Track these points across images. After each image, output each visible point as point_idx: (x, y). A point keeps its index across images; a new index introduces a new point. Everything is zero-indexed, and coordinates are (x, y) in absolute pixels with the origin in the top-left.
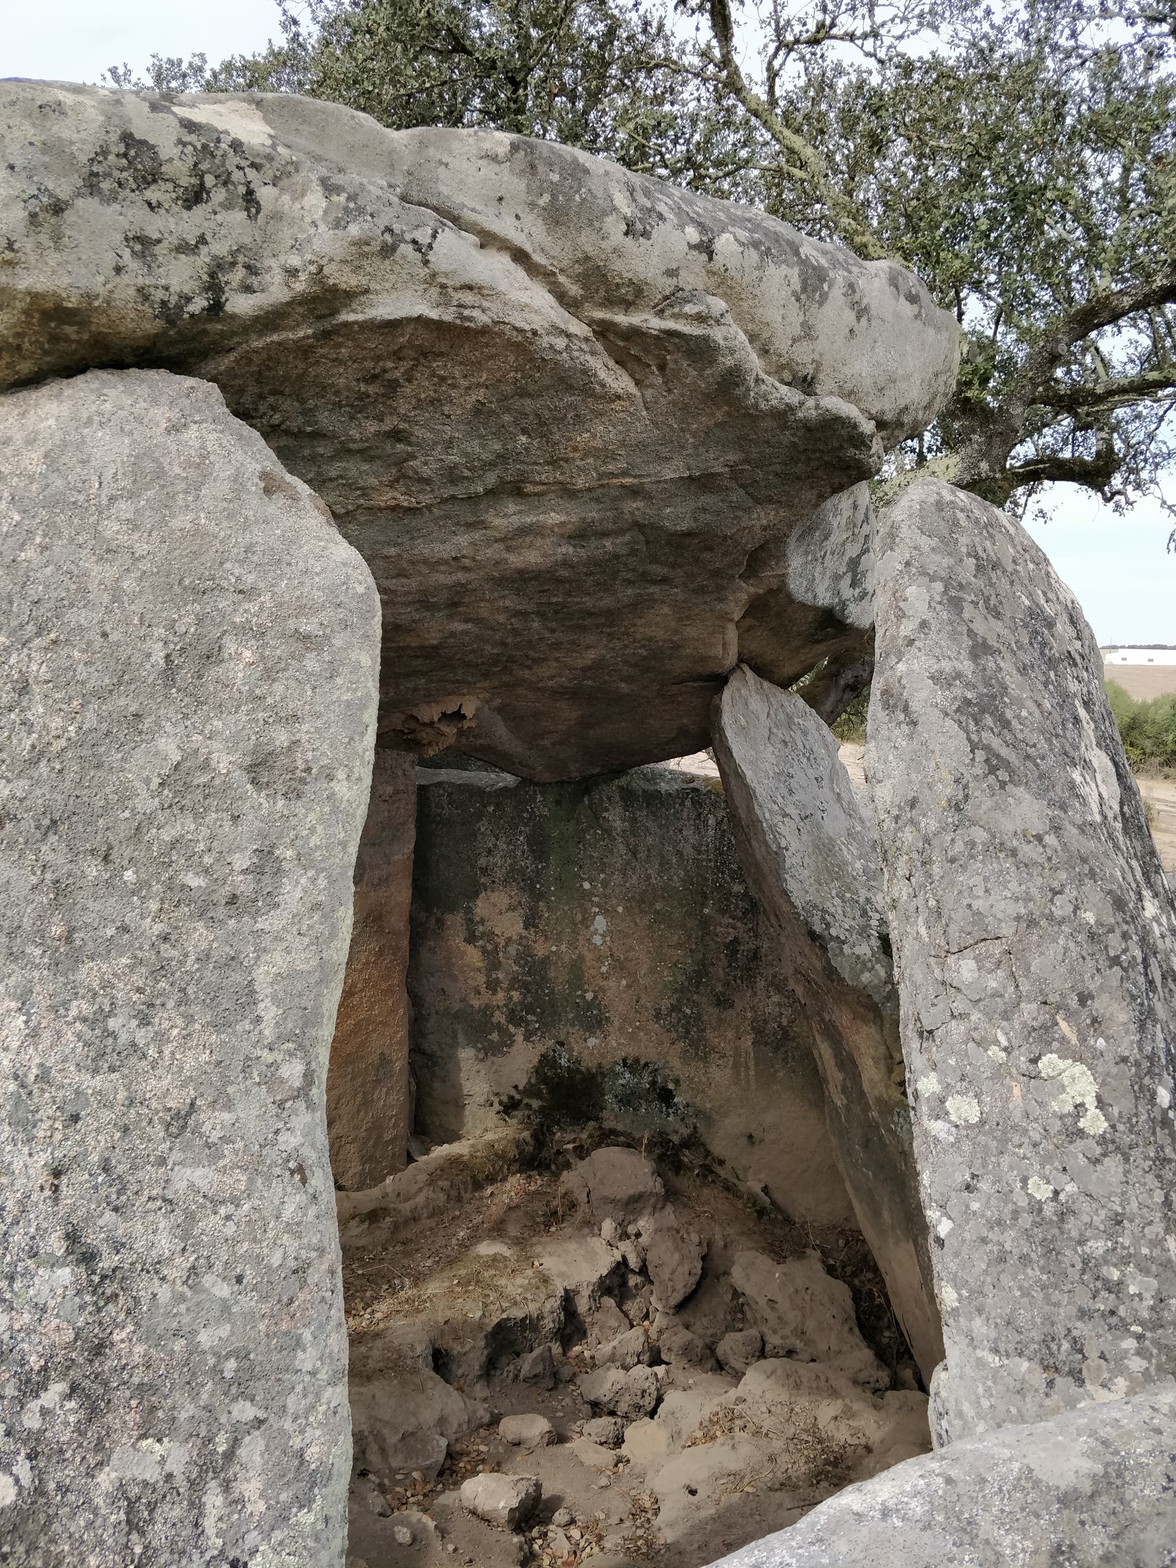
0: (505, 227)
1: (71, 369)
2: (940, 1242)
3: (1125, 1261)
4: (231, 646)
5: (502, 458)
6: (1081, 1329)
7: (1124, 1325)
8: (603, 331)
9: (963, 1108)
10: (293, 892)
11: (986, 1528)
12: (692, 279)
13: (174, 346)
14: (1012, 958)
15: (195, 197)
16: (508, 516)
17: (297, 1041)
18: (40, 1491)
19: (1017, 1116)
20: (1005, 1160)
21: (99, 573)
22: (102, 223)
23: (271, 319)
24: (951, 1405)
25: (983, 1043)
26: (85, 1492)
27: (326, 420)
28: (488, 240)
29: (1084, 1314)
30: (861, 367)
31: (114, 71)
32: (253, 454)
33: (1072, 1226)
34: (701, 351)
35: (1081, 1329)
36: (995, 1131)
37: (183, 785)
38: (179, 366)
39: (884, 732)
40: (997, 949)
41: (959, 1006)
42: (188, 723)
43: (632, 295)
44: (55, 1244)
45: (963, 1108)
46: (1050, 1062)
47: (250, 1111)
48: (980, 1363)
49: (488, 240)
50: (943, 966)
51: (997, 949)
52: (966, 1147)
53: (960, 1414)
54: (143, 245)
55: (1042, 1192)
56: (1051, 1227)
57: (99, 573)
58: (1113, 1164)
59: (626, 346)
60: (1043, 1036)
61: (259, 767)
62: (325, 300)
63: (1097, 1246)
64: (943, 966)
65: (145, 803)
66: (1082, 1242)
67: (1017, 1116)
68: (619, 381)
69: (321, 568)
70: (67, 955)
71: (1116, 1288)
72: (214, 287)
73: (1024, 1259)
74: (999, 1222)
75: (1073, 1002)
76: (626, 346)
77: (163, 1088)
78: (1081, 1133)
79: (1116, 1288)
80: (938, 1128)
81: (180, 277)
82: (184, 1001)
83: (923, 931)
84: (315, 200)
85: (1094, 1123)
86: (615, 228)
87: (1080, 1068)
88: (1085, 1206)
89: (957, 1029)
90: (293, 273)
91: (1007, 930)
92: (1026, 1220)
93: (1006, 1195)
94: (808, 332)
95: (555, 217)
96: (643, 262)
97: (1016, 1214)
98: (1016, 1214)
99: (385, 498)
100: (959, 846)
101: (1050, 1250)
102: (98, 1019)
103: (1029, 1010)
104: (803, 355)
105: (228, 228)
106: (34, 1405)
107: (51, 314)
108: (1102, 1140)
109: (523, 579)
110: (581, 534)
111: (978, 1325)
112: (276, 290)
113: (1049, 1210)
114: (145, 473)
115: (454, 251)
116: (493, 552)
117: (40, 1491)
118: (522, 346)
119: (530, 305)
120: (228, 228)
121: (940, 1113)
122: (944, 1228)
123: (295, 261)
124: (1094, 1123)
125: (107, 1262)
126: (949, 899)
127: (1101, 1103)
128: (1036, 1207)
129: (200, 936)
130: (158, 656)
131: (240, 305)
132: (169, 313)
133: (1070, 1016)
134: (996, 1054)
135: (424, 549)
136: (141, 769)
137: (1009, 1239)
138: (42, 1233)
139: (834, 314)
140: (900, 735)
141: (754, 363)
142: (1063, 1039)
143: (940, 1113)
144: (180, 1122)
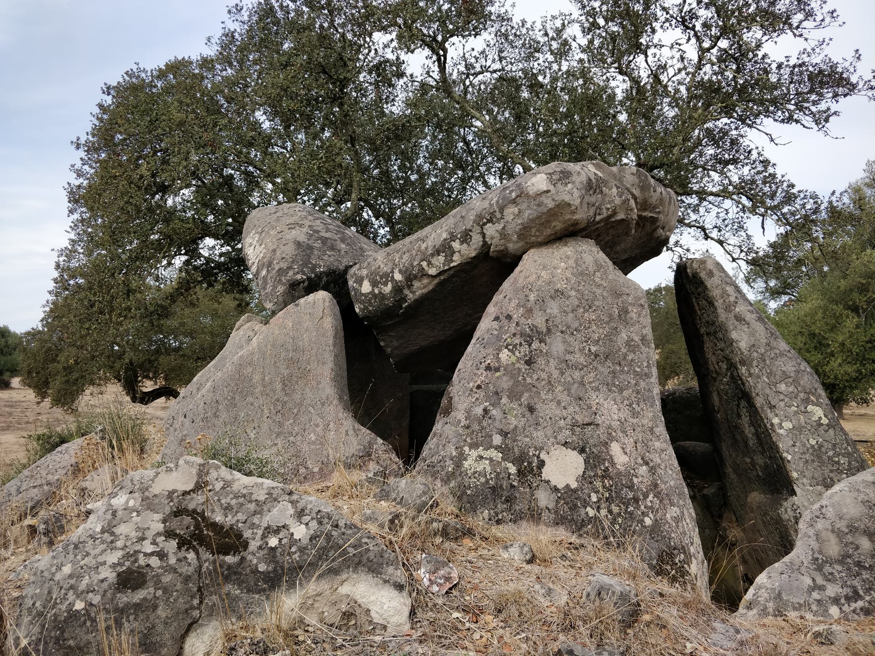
2: (788, 461)
3: (839, 455)
4: (630, 309)
6: (831, 475)
7: (842, 472)
9: (787, 425)
11: (862, 489)
14: (796, 382)
18: (656, 520)
19: (803, 424)
20: (802, 436)
21: (598, 291)
24: (800, 505)
25: (789, 407)
26: (665, 519)
29: (831, 471)
31: (127, 73)
33: (823, 449)
35: (831, 475)
36: (798, 429)
39: (739, 327)
40: (791, 380)
41: (782, 397)
44: (640, 461)
45: (787, 425)
46: (810, 408)
48: (808, 490)
50: (775, 387)
51: (791, 380)
52: (790, 435)
53: (804, 506)
55: (813, 442)
56: (818, 451)
57: (598, 291)
58: (831, 432)
60: (807, 401)
63: (831, 453)
64: (775, 387)
65: (624, 350)
66: (827, 453)
67: (803, 424)
71: (838, 463)
73: (813, 461)
74: (804, 453)
75: (813, 391)
78: (822, 424)
79: (838, 463)
80: (781, 431)
82: (644, 400)
83: (766, 380)
84: (614, 190)
85: (825, 421)
87: (818, 408)
88: (825, 444)
89: (782, 404)
90: (608, 209)
91: (792, 375)
92: (811, 451)
93: (804, 445)
97: (808, 450)
98: (808, 450)
100: (773, 355)
101: (819, 457)
102: (630, 405)
103: (802, 395)
106: (648, 500)
108: (827, 425)
111: (805, 481)
113: (816, 447)
117: (656, 520)
121: (781, 427)
122: (789, 457)
123: (609, 206)
124: (825, 421)
125: (651, 464)
126: (774, 369)
127: (825, 416)
128: (813, 447)
130: (617, 312)
133: (813, 395)
134: (794, 409)
137: (807, 456)
138: (636, 458)
140: (745, 328)
142: (813, 401)
143: (781, 427)
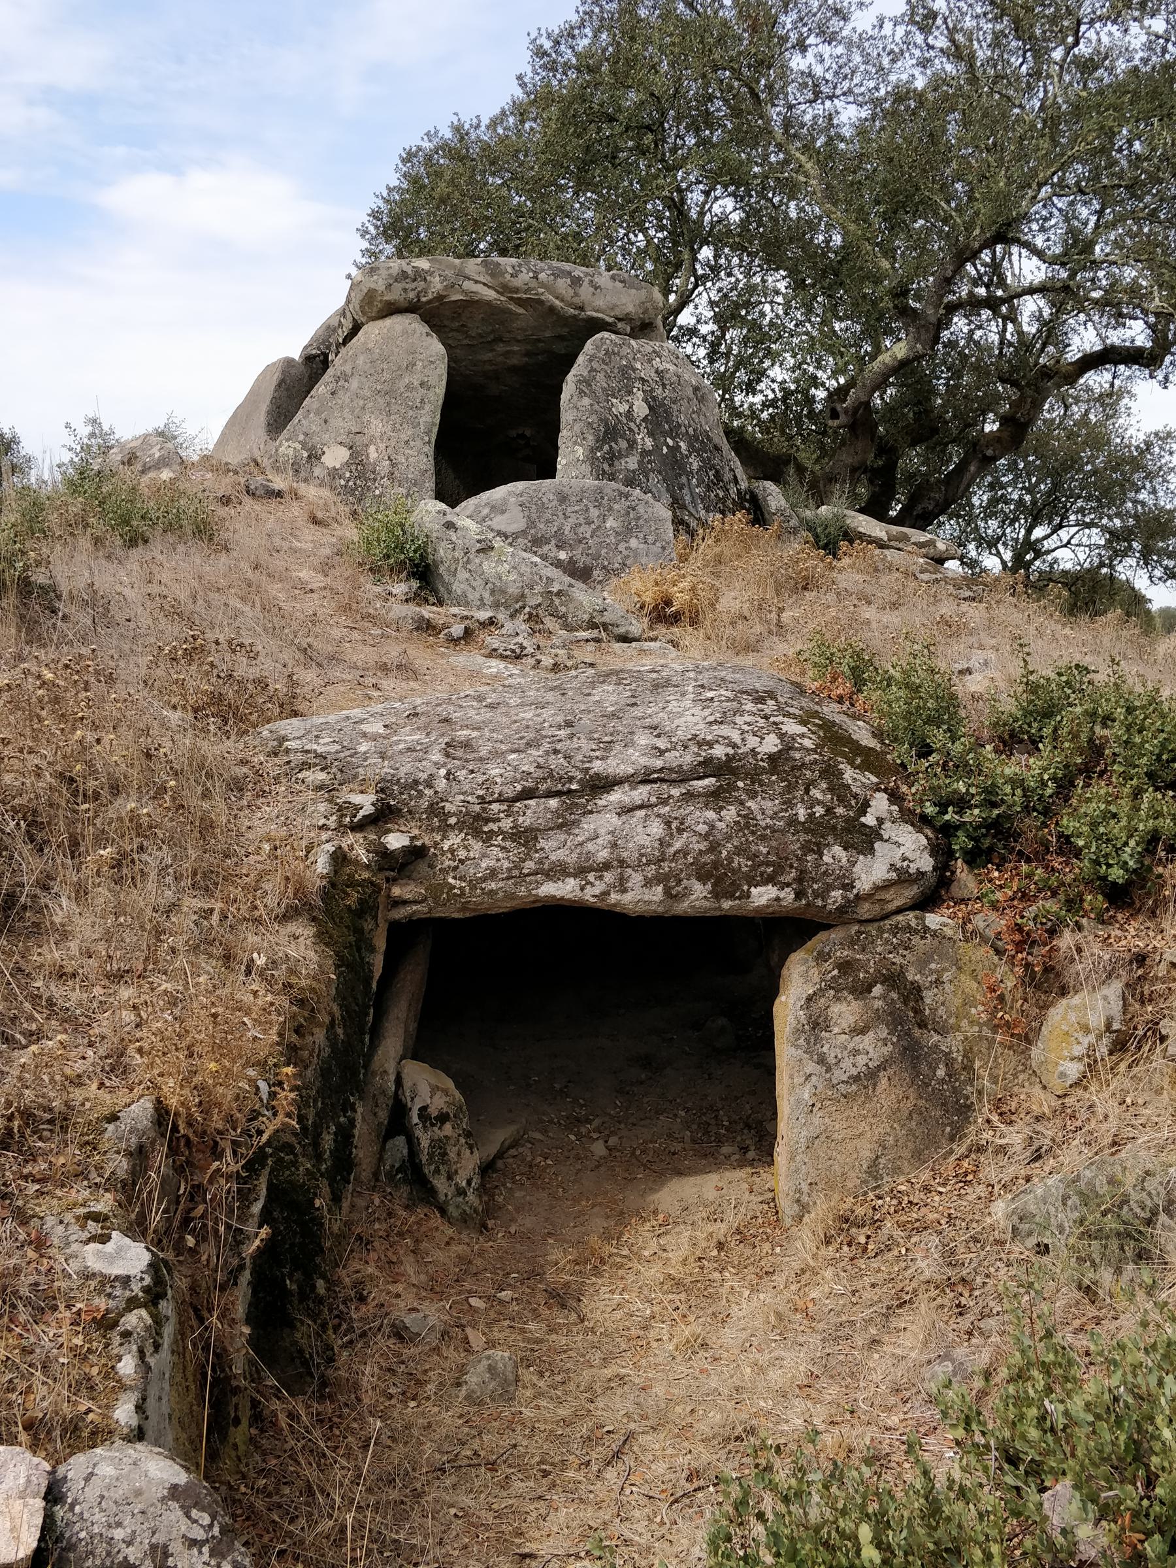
0: (481, 279)
1: (392, 314)
5: (493, 331)
8: (511, 299)
10: (427, 407)
12: (533, 284)
13: (411, 308)
15: (415, 280)
16: (501, 348)
17: (428, 433)
22: (398, 287)
23: (430, 302)
27: (446, 323)
28: (476, 282)
30: (600, 302)
32: (427, 329)
34: (540, 302)
37: (409, 387)
38: (412, 312)
42: (992, 1270)
43: (517, 290)
47: (419, 443)
49: (476, 282)
54: (405, 290)
59: (520, 302)
61: (422, 384)
62: (440, 298)
68: (521, 311)
69: (436, 347)
70: (389, 414)
72: (418, 296)
76: (520, 302)
77: (404, 437)
81: (412, 295)
86: (508, 277)
94: (576, 294)
95: (492, 275)
96: (518, 282)
99: (465, 342)
104: (576, 300)
105: (421, 285)
107: (389, 304)
109: (514, 369)
110: (527, 354)
112: (430, 296)
114: (405, 332)
115: (468, 285)
116: (501, 359)
118: (489, 303)
119: (491, 295)
120: (421, 285)
129: (411, 413)
131: (424, 299)
132: (410, 302)
135: (479, 357)
136: (401, 385)
139: (585, 291)
141: (557, 302)
144: (407, 442)
